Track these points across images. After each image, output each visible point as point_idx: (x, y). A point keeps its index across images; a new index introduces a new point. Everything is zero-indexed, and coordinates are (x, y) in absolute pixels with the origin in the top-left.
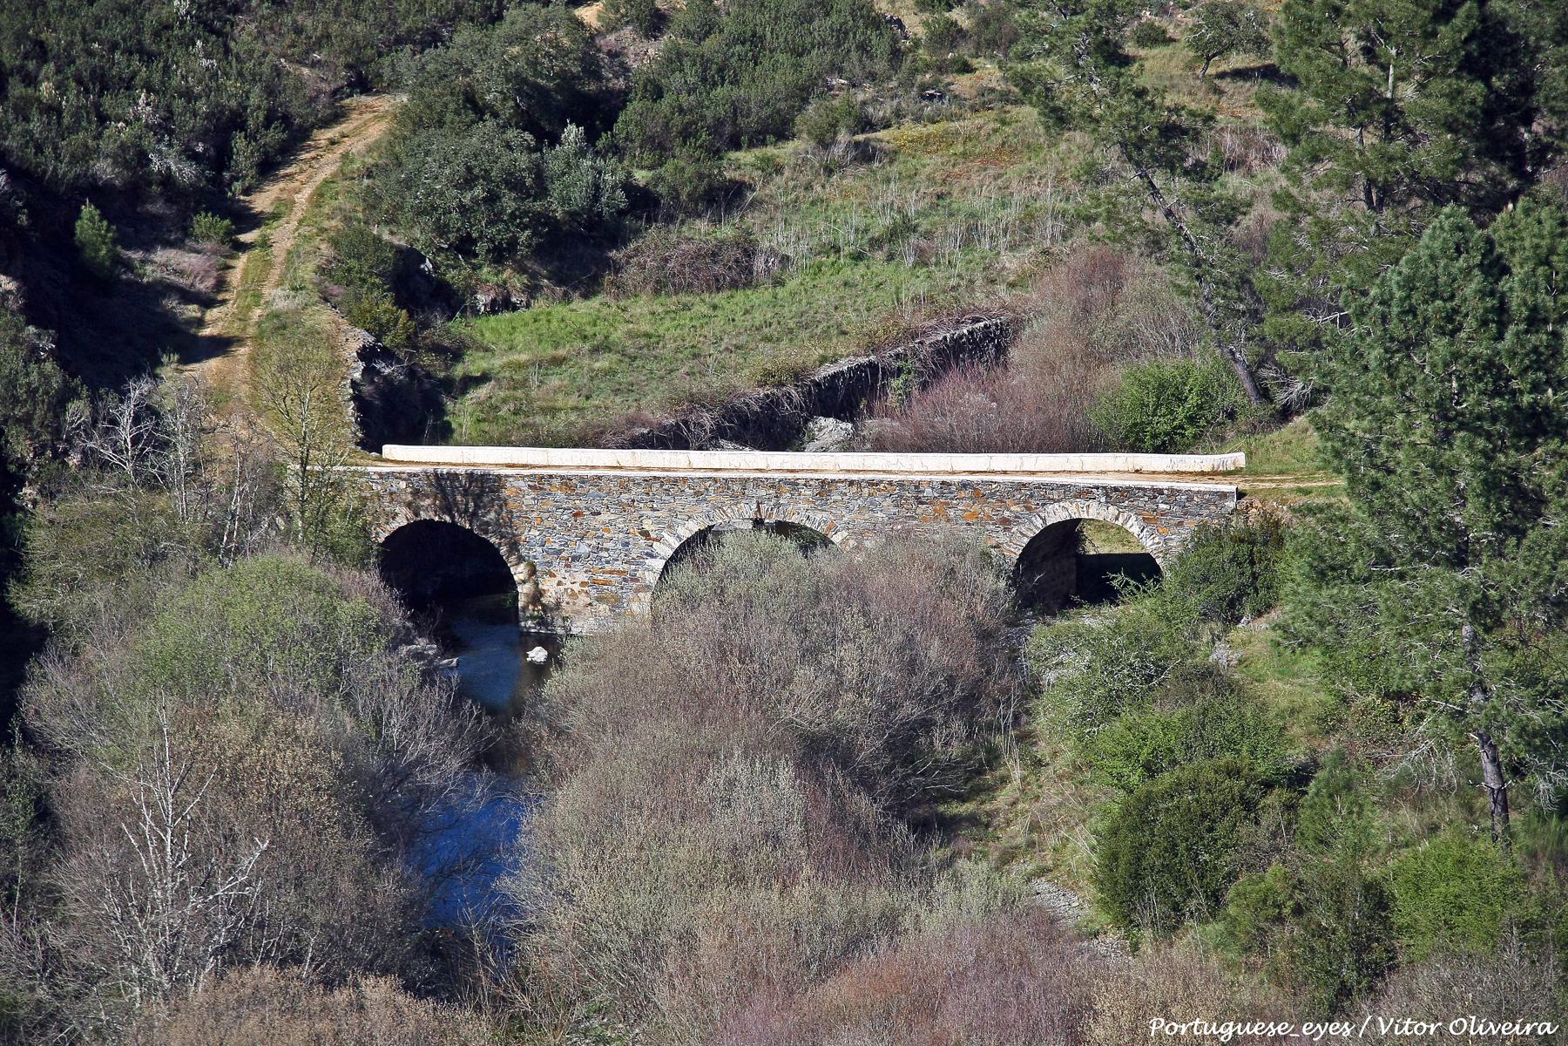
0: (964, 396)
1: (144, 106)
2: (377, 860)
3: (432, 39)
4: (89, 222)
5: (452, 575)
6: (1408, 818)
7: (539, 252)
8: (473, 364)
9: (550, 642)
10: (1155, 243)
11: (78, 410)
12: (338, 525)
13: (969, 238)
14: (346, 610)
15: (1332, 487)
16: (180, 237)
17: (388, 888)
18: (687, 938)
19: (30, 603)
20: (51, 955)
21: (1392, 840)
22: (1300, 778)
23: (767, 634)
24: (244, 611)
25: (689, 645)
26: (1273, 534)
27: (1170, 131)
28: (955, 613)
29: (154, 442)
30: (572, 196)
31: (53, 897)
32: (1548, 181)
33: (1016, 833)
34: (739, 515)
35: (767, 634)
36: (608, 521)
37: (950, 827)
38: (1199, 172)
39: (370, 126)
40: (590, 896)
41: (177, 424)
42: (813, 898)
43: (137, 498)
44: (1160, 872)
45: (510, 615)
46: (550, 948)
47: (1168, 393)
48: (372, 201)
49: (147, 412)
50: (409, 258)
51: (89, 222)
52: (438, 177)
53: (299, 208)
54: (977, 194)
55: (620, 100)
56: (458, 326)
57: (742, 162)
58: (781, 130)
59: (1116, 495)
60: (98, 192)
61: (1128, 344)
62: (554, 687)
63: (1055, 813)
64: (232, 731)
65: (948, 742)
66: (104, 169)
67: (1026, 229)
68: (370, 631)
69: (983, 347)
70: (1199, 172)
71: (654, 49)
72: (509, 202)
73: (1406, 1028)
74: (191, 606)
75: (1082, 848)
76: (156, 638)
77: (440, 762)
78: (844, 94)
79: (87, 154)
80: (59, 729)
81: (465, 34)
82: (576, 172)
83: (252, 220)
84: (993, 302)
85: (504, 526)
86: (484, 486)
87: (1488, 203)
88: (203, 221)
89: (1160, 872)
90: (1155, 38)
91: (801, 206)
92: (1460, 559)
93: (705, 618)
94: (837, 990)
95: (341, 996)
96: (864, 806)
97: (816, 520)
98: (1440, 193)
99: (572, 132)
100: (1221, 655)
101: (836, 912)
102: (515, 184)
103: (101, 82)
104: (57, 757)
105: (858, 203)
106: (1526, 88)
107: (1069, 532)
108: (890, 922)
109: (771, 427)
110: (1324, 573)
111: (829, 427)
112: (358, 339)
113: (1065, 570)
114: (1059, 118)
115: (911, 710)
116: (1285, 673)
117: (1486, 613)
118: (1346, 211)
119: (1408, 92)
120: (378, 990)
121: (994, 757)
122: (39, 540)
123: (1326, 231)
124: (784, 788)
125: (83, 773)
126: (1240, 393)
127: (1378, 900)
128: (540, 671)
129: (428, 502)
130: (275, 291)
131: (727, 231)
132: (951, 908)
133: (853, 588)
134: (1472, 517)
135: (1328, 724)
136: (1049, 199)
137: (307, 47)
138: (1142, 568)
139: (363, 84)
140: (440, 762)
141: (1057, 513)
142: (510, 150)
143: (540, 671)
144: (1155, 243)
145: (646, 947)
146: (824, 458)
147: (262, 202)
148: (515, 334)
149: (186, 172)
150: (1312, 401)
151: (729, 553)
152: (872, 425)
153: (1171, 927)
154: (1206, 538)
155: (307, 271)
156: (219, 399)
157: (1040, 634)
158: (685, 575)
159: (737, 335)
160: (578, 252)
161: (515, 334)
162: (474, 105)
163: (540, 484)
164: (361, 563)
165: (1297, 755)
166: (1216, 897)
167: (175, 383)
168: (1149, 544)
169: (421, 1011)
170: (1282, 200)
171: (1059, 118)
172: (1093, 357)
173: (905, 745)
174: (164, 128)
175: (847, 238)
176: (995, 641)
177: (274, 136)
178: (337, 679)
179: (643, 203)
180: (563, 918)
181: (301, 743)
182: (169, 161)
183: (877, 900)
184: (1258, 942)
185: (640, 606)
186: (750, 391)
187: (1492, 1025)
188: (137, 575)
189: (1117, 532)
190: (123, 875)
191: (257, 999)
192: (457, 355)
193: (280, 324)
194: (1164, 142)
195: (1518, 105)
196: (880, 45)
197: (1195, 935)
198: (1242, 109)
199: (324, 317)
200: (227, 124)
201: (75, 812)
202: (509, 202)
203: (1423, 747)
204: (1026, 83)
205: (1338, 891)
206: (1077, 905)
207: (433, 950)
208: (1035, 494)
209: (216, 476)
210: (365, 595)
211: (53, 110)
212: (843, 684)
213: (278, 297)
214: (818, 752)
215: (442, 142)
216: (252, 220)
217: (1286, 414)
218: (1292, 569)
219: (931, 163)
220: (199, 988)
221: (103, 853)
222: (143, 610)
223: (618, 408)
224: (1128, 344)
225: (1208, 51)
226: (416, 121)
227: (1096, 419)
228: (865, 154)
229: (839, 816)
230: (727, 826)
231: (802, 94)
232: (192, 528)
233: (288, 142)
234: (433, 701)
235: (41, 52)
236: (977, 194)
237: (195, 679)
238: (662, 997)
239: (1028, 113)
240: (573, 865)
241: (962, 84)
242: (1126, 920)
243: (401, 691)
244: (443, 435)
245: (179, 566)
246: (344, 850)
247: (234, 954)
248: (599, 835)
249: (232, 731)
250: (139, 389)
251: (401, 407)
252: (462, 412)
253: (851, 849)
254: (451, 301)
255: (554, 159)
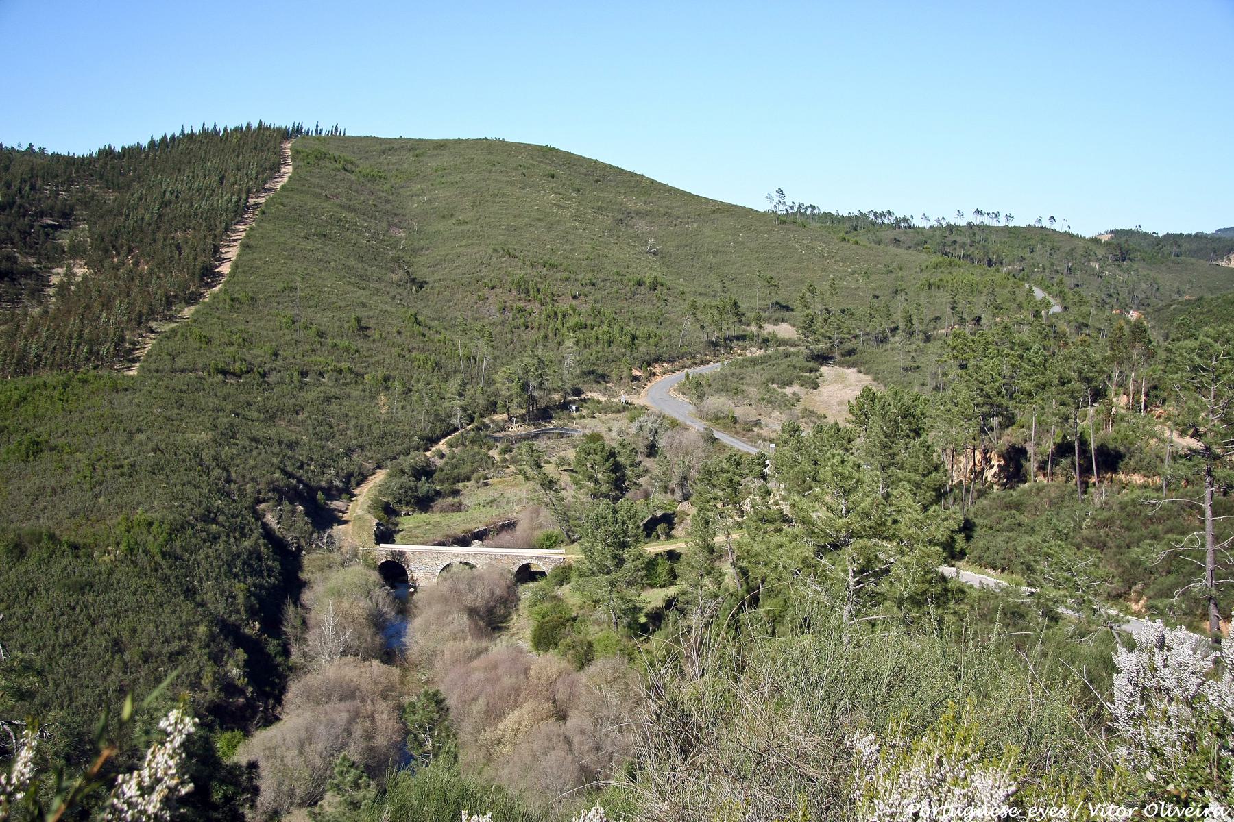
0: (506, 536)
1: (332, 471)
2: (375, 634)
3: (395, 458)
4: (320, 495)
5: (394, 572)
6: (597, 628)
7: (416, 504)
8: (400, 527)
9: (415, 587)
10: (547, 505)
11: (315, 535)
12: (370, 561)
13: (508, 502)
14: (371, 579)
15: (582, 557)
16: (338, 498)
17: (378, 640)
18: (442, 652)
19: (303, 576)
20: (305, 653)
21: (593, 632)
22: (574, 619)
23: (462, 586)
24: (348, 580)
25: (445, 588)
26: (570, 567)
27: (551, 482)
28: (503, 583)
29: (331, 541)
30: (423, 492)
31: (306, 640)
32: (628, 495)
33: (514, 630)
34: (457, 561)
35: (462, 586)
36: (427, 564)
37: (500, 629)
38: (556, 491)
39: (380, 476)
40: (422, 643)
41: (336, 539)
42: (471, 643)
43: (327, 555)
44: (545, 638)
45: (406, 581)
46: (413, 653)
47: (549, 537)
48: (380, 492)
49: (330, 536)
50: (387, 504)
51: (320, 495)
52: (394, 487)
53: (365, 493)
54: (510, 493)
55: (434, 472)
56: (397, 519)
57: (460, 486)
58: (468, 479)
59: (538, 558)
60: (322, 489)
61: (540, 526)
62: (415, 597)
63: (523, 625)
64: (345, 605)
65: (500, 611)
66: (323, 484)
67: (520, 501)
68: (375, 584)
69: (510, 526)
70: (556, 491)
71: (442, 461)
72: (410, 493)
73: (1110, 811)
74: (337, 578)
75: (528, 633)
76: (329, 585)
77: (390, 612)
78: (481, 472)
79: (320, 481)
80: (308, 603)
81: (402, 457)
82: (424, 487)
83: (355, 496)
84: (512, 516)
85: (407, 562)
86: (402, 554)
87: (616, 499)
88: (344, 495)
89: (545, 638)
90: (547, 462)
91: (472, 494)
92: (608, 573)
93: (448, 584)
94: (475, 663)
95: (367, 663)
96: (481, 623)
97: (473, 562)
98: (606, 496)
99: (423, 478)
100: (559, 593)
101: (474, 646)
102: (411, 489)
103: (324, 466)
104: (308, 610)
105: (484, 495)
106: (624, 476)
107: (527, 566)
108: (486, 649)
109: (464, 541)
110: (580, 576)
111: (476, 542)
112: (376, 521)
113: (526, 574)
114: (527, 479)
115: (492, 604)
116: (573, 596)
117: (613, 584)
118: (587, 499)
119: (600, 476)
120: (375, 662)
121: (510, 614)
122: (306, 563)
123: (583, 503)
124: (463, 620)
125: (313, 614)
126: (564, 537)
127: (590, 645)
128: (412, 594)
129: (174, 715)
130: (359, 511)
131: (456, 500)
132: (499, 647)
133: (481, 577)
134: (610, 563)
135: (581, 608)
136: (525, 495)
137: (368, 459)
138: (543, 574)
139: (379, 467)
140: (390, 612)
141: (525, 562)
142: (408, 481)
143: (412, 594)
144: (547, 505)
145: (434, 654)
146: (476, 548)
147: (356, 492)
148: (410, 521)
149: (340, 485)
150: (579, 539)
151: (454, 569)
152: (486, 542)
153: (547, 650)
154: (557, 568)
155: (365, 507)
156: (345, 533)
157: (521, 588)
158: (444, 574)
159: (457, 523)
160: (424, 503)
161: (410, 521)
162: (403, 472)
163: (414, 553)
164: (374, 569)
165: (574, 614)
166: (557, 645)
167: (337, 530)
168: (544, 569)
169: (384, 667)
170: (574, 497)
171: (527, 479)
172: (533, 529)
173: (491, 611)
174: (337, 475)
175: (482, 502)
176: (511, 589)
177: (360, 478)
178: (368, 594)
179: (438, 494)
180: (416, 647)
181: (360, 608)
182: (337, 483)
183: (483, 644)
184: (565, 654)
185: (435, 580)
186: (460, 534)
187: (1177, 809)
188: (327, 571)
189: (537, 566)
190: (321, 635)
191: (348, 664)
192: (397, 525)
193: (359, 518)
194: (549, 484)
195: (622, 479)
196: (490, 462)
197: (552, 653)
198: (565, 478)
199: (369, 516)
200: (350, 476)
201: (311, 621)
202: (410, 493)
203: (600, 613)
204: (520, 471)
205: (582, 643)
206: (526, 645)
207: (388, 654)
208: (521, 558)
209: (344, 550)
210: (375, 576)
211: (313, 471)
212: (479, 596)
213: (359, 512)
214: (472, 612)
215: (396, 480)
216: (355, 496)
217: (573, 542)
218: (574, 574)
219: (500, 487)
220: (336, 661)
221: (316, 631)
222: (327, 578)
223: (432, 537)
224: (540, 526)
225: (559, 465)
226: (391, 475)
227: (534, 542)
228: (486, 485)
229: (476, 625)
230: (455, 627)
231: (473, 472)
232: (338, 561)
233: (363, 478)
234: (388, 600)
235: (312, 459)
236: (510, 493)
237: (338, 594)
238: (436, 664)
239: (521, 477)
240: (418, 635)
241: (507, 470)
242: (537, 649)
243: (382, 596)
244: (393, 542)
245: (334, 569)
246: (368, 632)
247: (344, 653)
248: (425, 631)
249: (345, 605)
250: (328, 531)
251: (384, 536)
252: (397, 537)
253: (480, 634)
254: (396, 513)
255: (420, 484)
